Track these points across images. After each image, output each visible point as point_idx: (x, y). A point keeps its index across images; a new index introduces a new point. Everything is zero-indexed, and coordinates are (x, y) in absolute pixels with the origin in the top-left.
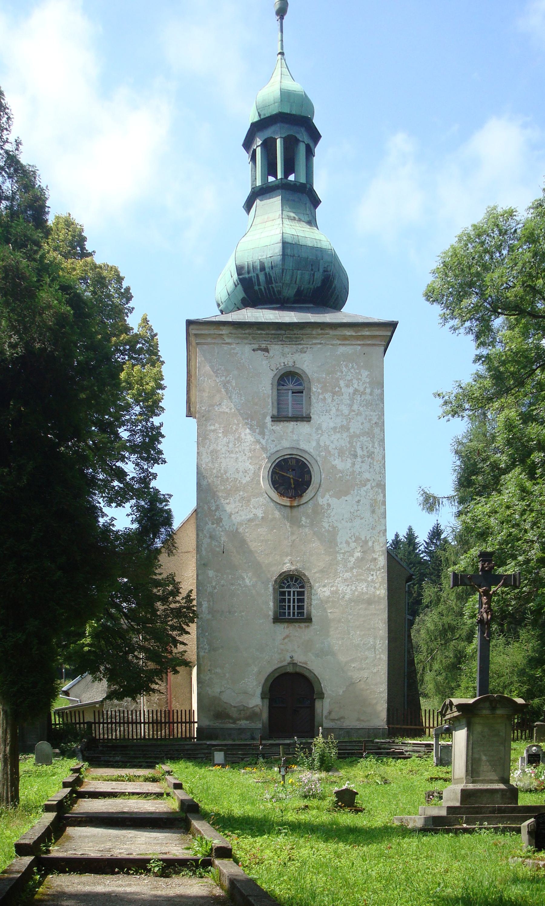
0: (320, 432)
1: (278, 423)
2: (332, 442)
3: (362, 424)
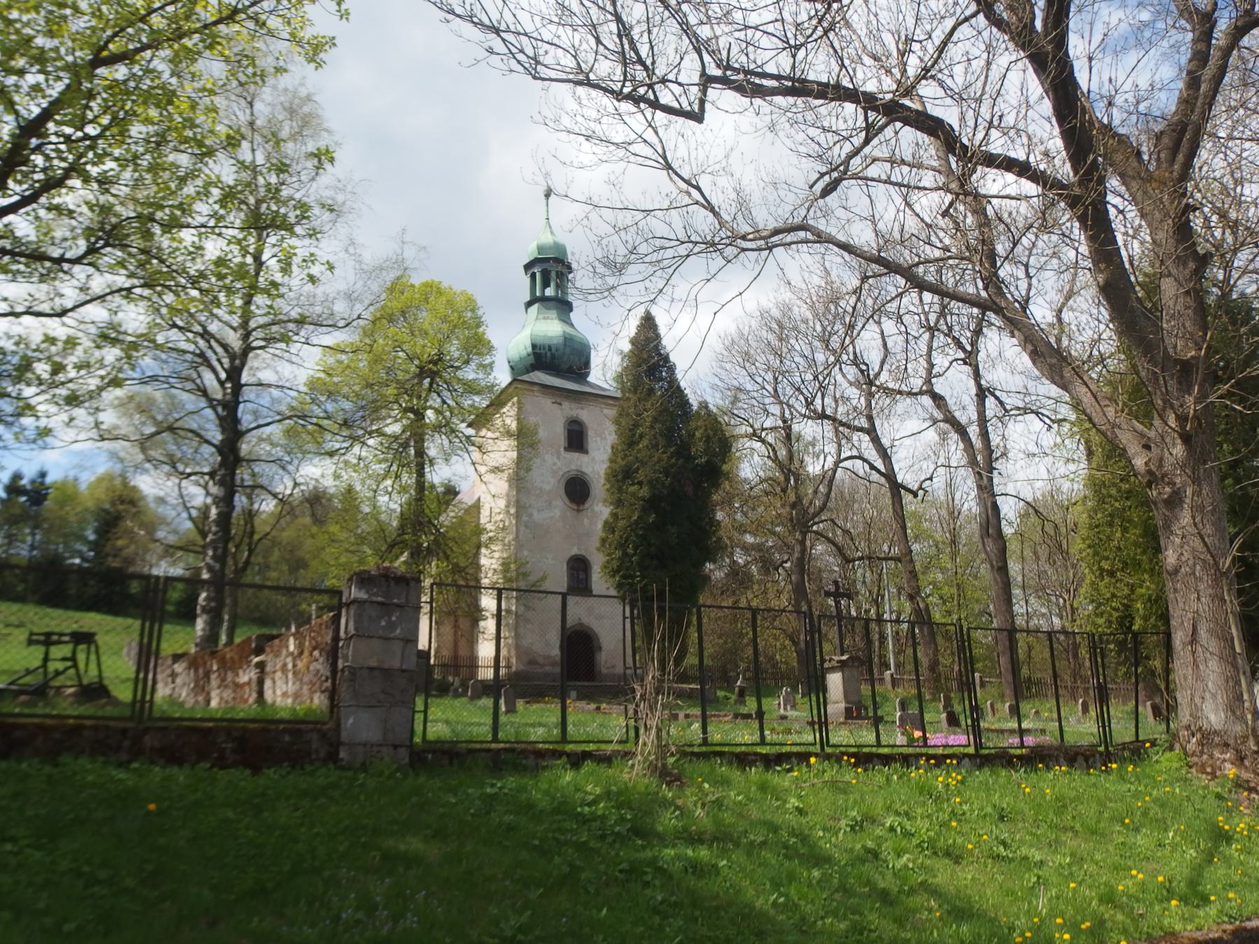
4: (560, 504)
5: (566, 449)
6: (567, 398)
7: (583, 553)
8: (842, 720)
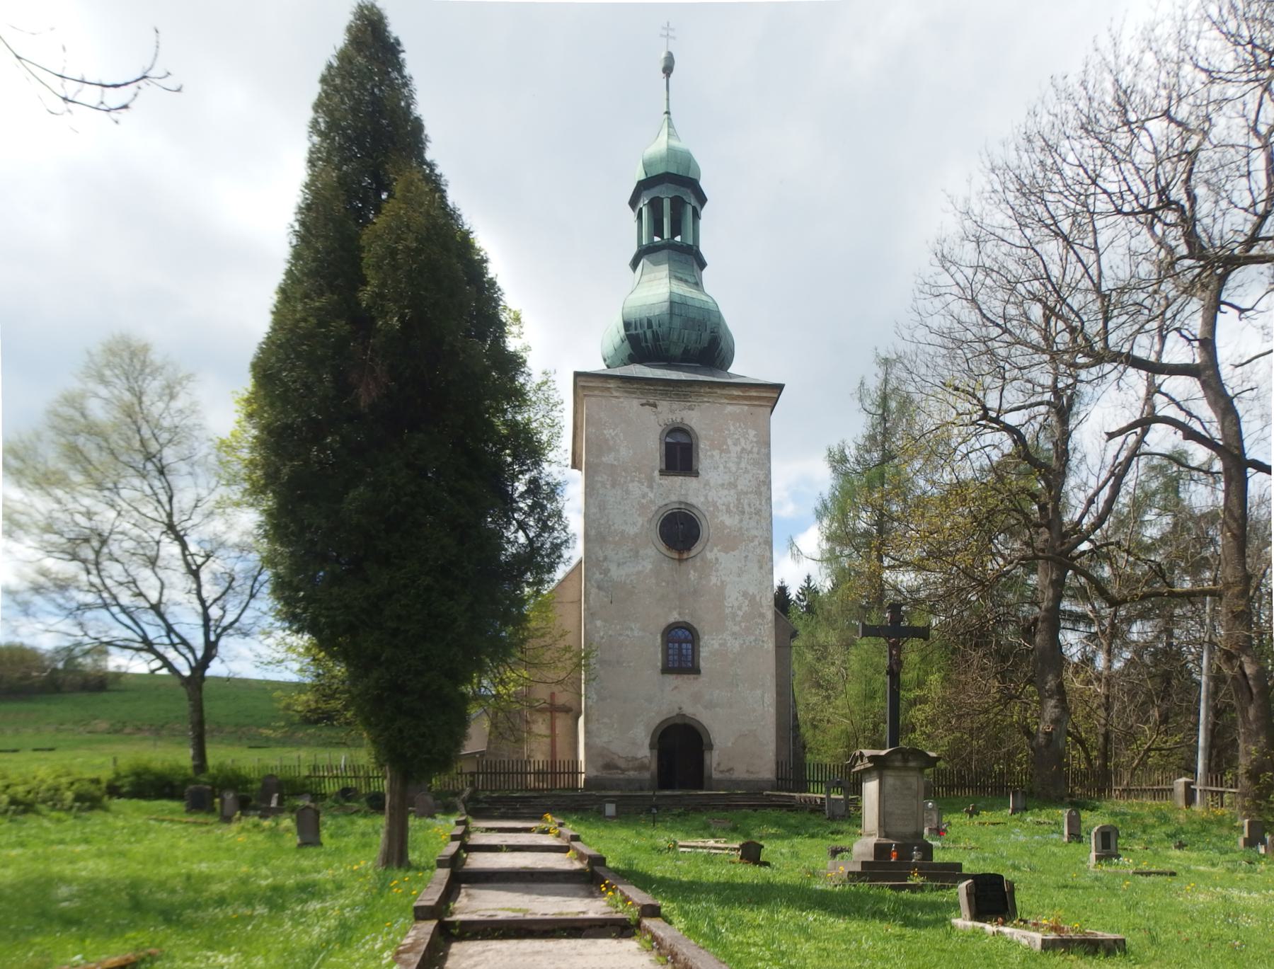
4: (653, 553)
5: (662, 473)
6: (665, 394)
7: (687, 619)
8: (302, 650)
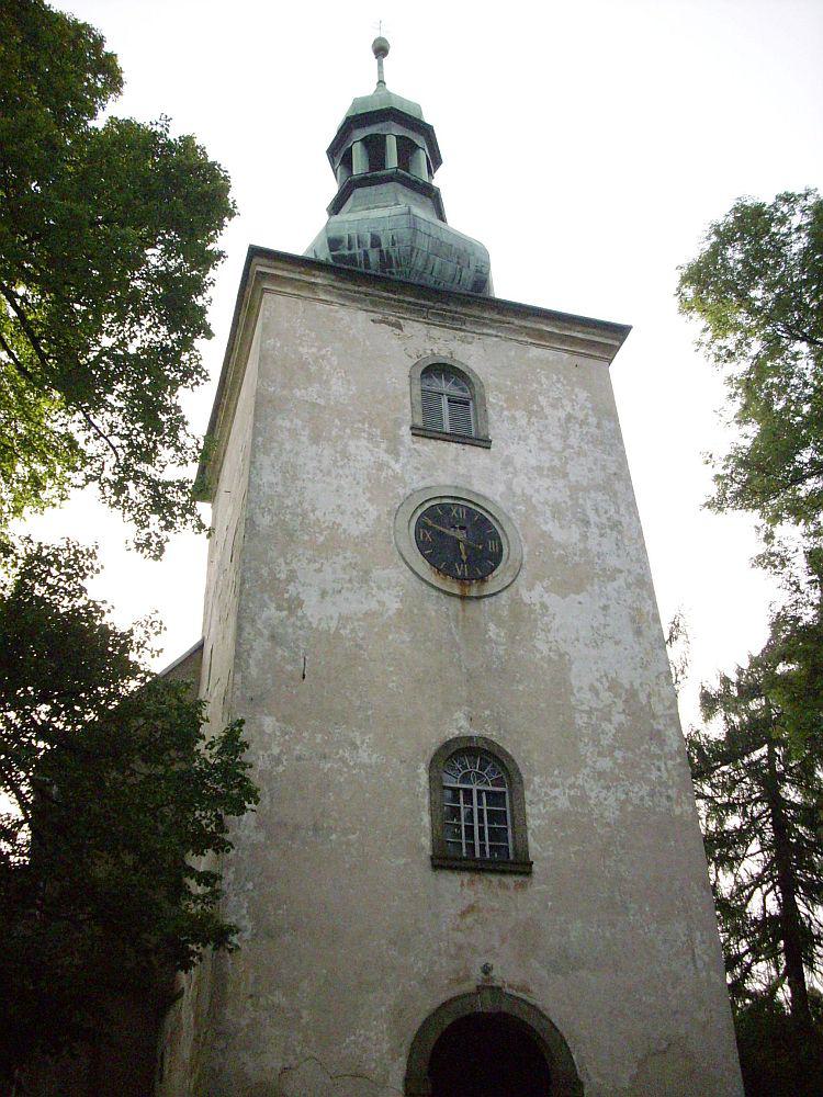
0: (510, 469)
1: (426, 440)
2: (538, 491)
3: (590, 470)
4: (397, 586)
